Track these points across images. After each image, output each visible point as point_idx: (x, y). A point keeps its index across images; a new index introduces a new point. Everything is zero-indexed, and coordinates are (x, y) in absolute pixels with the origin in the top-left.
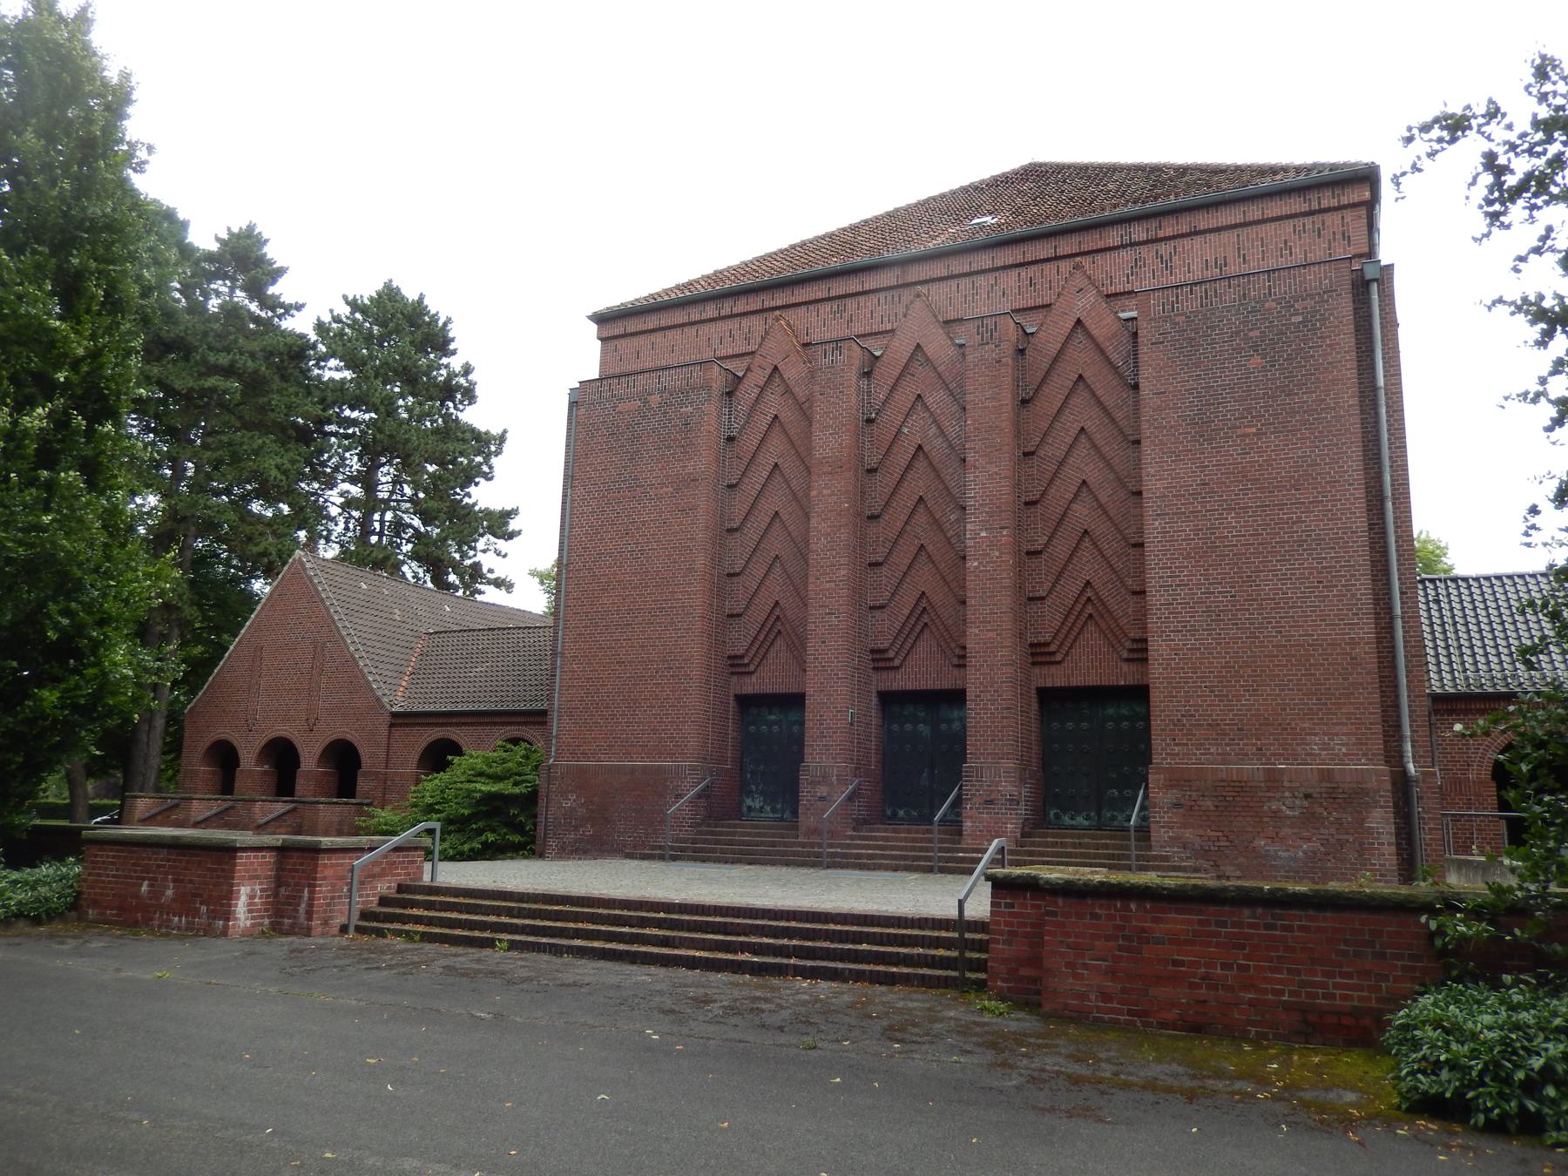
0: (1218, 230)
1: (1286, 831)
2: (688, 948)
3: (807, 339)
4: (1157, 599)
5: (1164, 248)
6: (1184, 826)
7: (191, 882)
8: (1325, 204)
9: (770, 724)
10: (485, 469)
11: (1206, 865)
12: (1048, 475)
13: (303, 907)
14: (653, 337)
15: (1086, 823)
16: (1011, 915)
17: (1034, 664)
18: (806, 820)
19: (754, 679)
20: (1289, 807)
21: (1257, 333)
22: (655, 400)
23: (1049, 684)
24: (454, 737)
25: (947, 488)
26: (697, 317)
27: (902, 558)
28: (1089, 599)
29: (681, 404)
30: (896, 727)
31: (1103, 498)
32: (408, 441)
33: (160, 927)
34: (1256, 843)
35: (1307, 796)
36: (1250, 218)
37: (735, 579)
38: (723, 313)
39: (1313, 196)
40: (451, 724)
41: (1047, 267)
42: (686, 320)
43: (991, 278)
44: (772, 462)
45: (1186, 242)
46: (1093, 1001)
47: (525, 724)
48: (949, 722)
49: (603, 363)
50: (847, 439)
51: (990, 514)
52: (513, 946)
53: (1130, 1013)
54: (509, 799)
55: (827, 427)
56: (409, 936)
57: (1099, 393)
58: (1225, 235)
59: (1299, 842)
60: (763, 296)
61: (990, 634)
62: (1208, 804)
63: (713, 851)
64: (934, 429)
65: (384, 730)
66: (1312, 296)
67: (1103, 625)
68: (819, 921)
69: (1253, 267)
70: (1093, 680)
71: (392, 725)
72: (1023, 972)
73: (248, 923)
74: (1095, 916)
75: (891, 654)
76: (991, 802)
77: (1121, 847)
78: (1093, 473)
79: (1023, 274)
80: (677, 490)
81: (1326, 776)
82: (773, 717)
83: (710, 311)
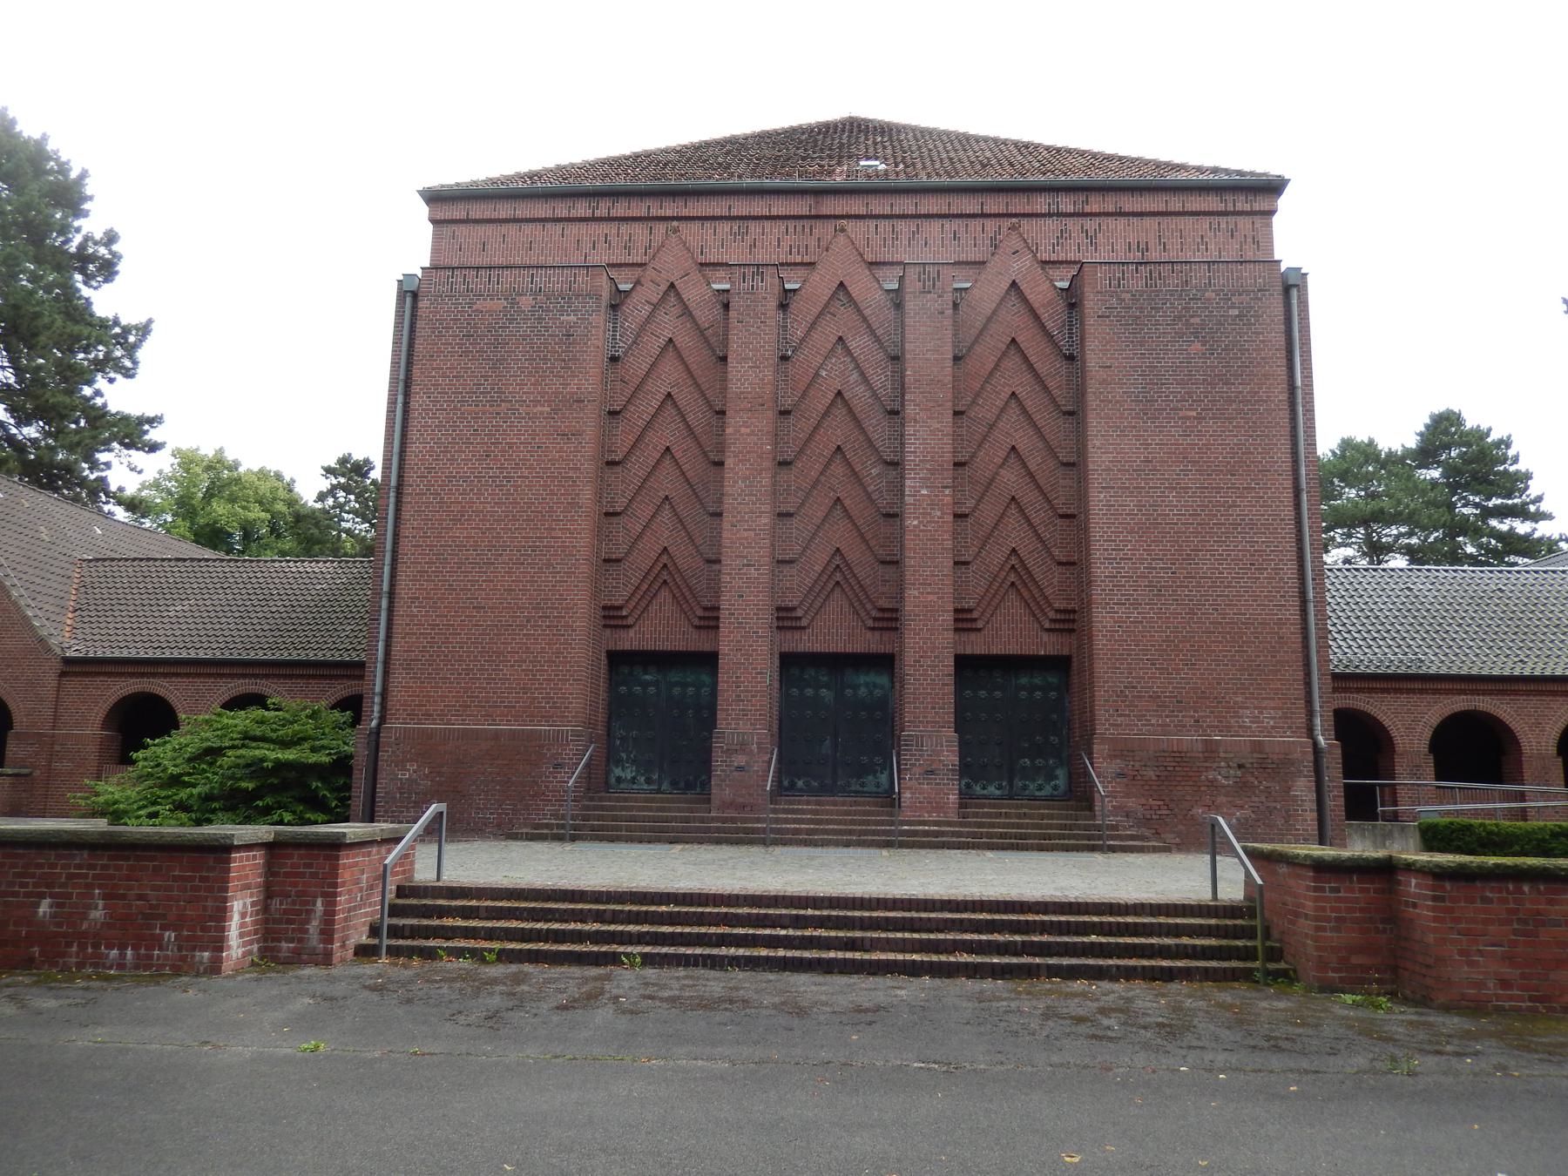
0: (1141, 214)
1: (1221, 799)
2: (883, 950)
3: (701, 259)
4: (1101, 570)
5: (1090, 224)
6: (1127, 795)
7: (140, 897)
8: (1239, 207)
9: (645, 685)
10: (128, 364)
11: (1147, 833)
12: (978, 437)
13: (314, 926)
14: (504, 228)
15: (998, 792)
16: (1339, 900)
17: (605, 626)
18: (721, 790)
19: (632, 633)
20: (1223, 777)
21: (1197, 320)
22: (526, 302)
23: (969, 651)
24: (161, 692)
25: (869, 440)
26: (565, 214)
27: (644, 511)
28: (1013, 567)
29: (562, 311)
30: (795, 692)
31: (1033, 467)
32: (37, 315)
33: (80, 965)
34: (1194, 811)
35: (1240, 766)
36: (1171, 208)
37: (614, 520)
38: (598, 213)
39: (1229, 197)
40: (154, 675)
41: (973, 223)
42: (549, 214)
43: (913, 225)
44: (664, 390)
45: (1110, 220)
46: (1492, 988)
47: (267, 676)
48: (855, 687)
49: (436, 250)
50: (769, 374)
51: (932, 471)
52: (648, 960)
53: (1531, 999)
54: (316, 769)
55: (745, 359)
56: (476, 954)
57: (1033, 359)
58: (1148, 221)
59: (1233, 810)
60: (648, 202)
61: (930, 598)
62: (1151, 774)
63: (619, 828)
64: (855, 376)
65: (51, 681)
66: (1248, 292)
67: (1025, 594)
68: (1013, 911)
69: (1172, 255)
70: (1012, 649)
71: (63, 674)
72: (1356, 960)
73: (240, 951)
74: (1485, 900)
75: (799, 613)
76: (932, 772)
77: (891, 815)
78: (1025, 440)
79: (947, 226)
80: (556, 411)
81: (1257, 747)
82: (648, 677)
83: (581, 209)
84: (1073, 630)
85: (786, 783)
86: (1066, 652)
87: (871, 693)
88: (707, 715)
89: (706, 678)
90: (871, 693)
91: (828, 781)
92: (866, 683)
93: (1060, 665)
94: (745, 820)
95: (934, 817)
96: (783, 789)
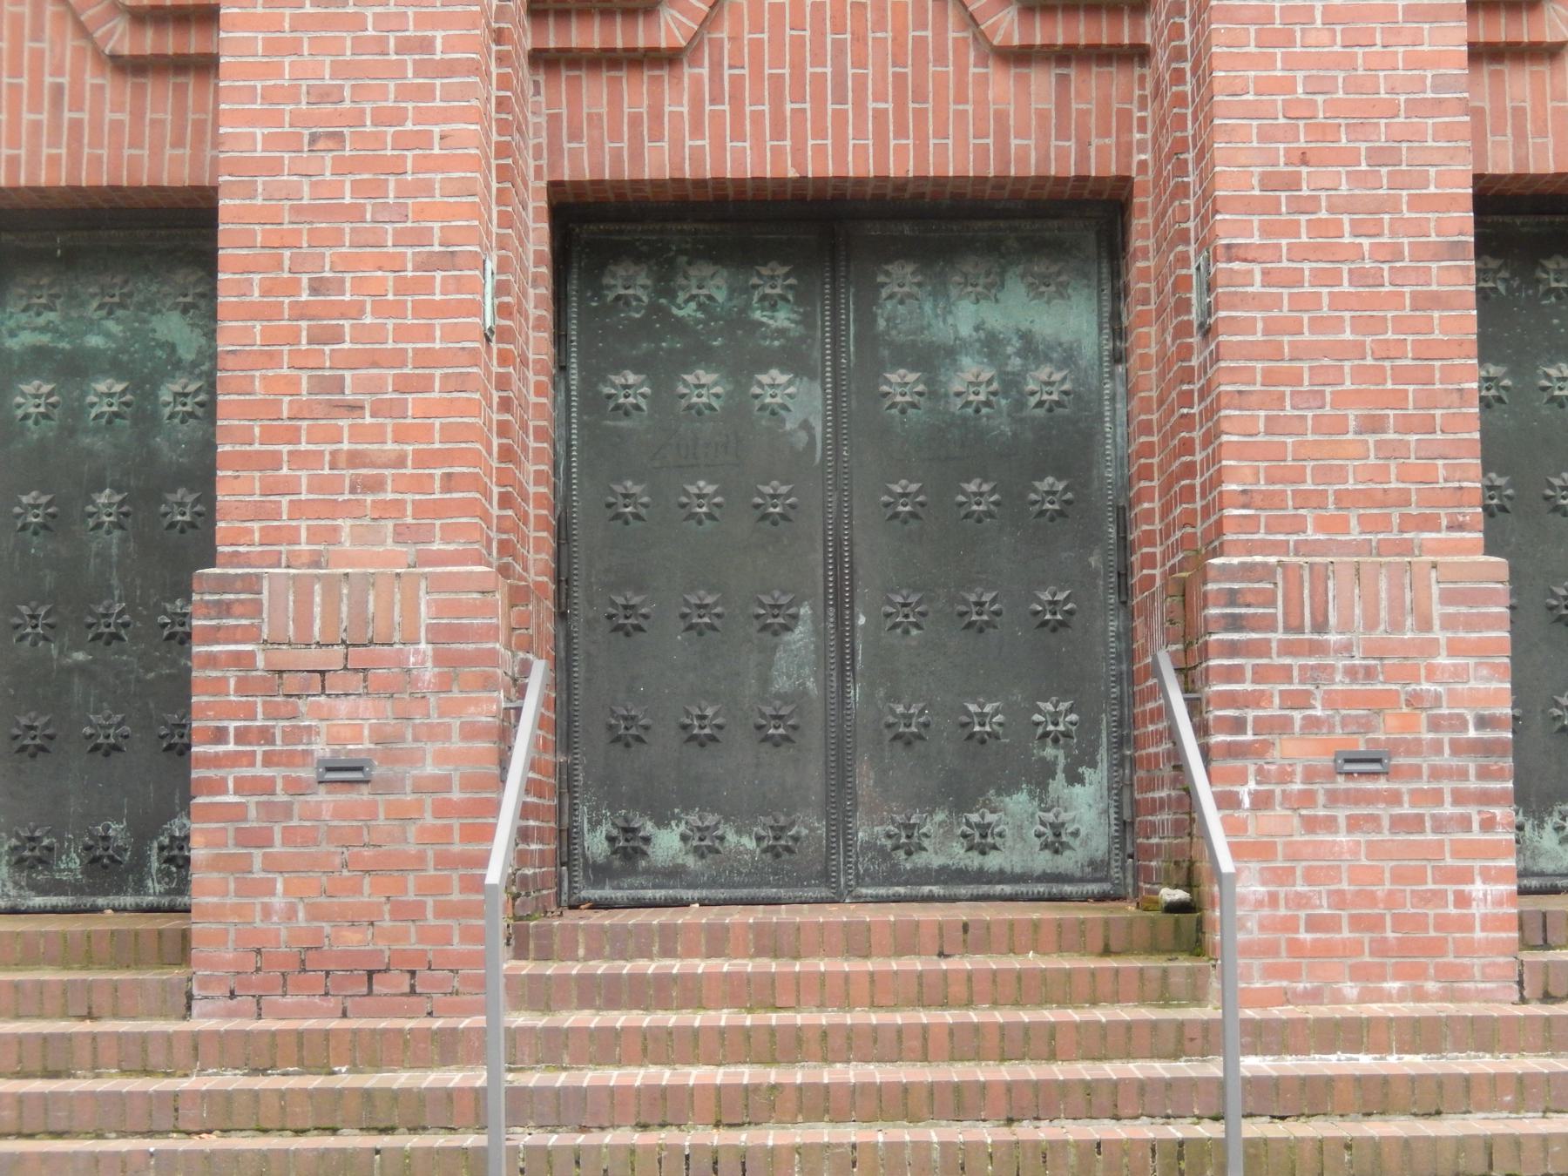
18: (243, 890)
48: (931, 359)
76: (1372, 762)
84: (1139, 54)
85: (596, 843)
86: (1101, 163)
87: (1011, 384)
88: (166, 513)
89: (172, 327)
90: (1011, 384)
91: (809, 826)
92: (991, 334)
93: (1075, 226)
94: (373, 1051)
95: (1393, 1003)
96: (585, 863)
